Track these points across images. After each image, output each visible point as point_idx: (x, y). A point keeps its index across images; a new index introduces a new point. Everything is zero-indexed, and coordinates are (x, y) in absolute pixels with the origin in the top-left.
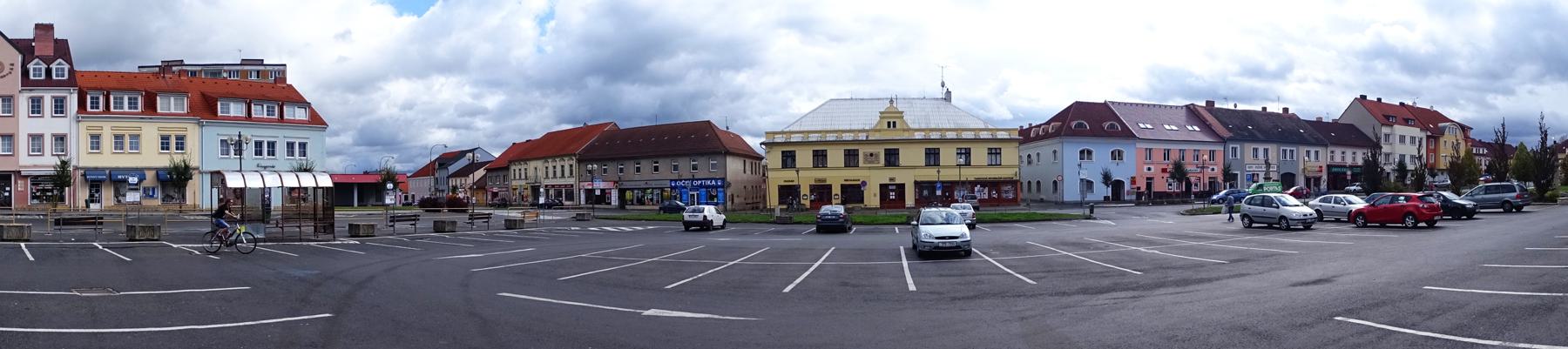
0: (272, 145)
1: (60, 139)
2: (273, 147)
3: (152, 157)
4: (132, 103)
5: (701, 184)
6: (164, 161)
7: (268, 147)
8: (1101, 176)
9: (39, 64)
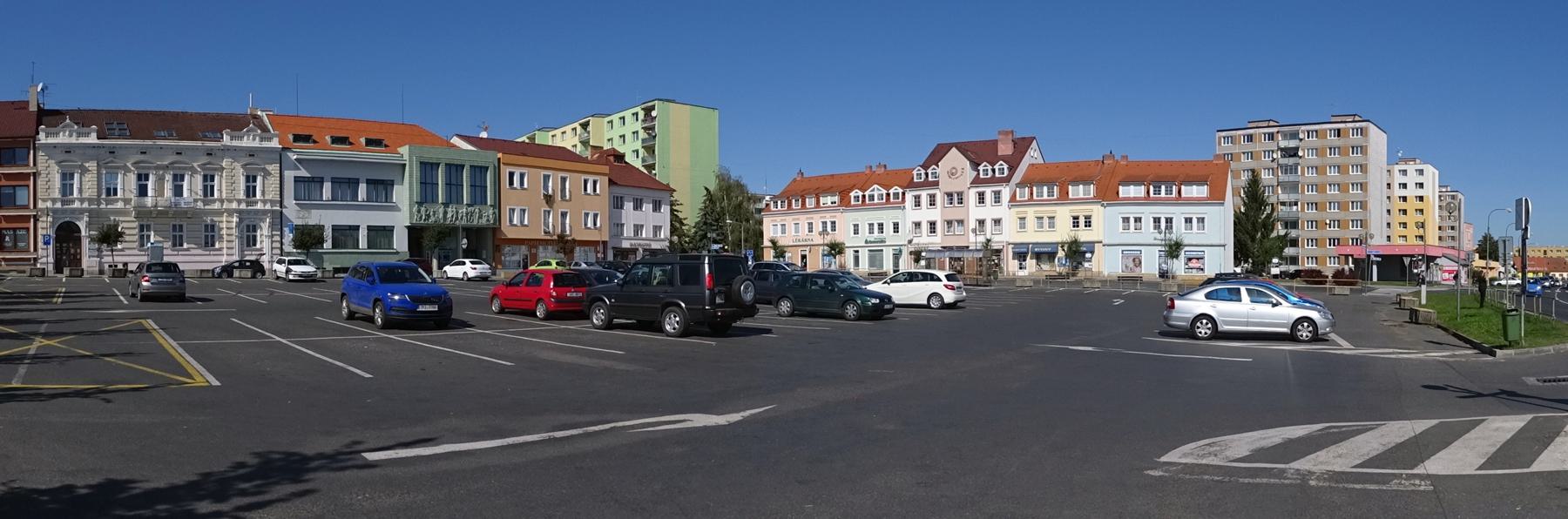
2: (1171, 222)
3: (1062, 233)
4: (1050, 193)
7: (1167, 222)
8: (841, 241)
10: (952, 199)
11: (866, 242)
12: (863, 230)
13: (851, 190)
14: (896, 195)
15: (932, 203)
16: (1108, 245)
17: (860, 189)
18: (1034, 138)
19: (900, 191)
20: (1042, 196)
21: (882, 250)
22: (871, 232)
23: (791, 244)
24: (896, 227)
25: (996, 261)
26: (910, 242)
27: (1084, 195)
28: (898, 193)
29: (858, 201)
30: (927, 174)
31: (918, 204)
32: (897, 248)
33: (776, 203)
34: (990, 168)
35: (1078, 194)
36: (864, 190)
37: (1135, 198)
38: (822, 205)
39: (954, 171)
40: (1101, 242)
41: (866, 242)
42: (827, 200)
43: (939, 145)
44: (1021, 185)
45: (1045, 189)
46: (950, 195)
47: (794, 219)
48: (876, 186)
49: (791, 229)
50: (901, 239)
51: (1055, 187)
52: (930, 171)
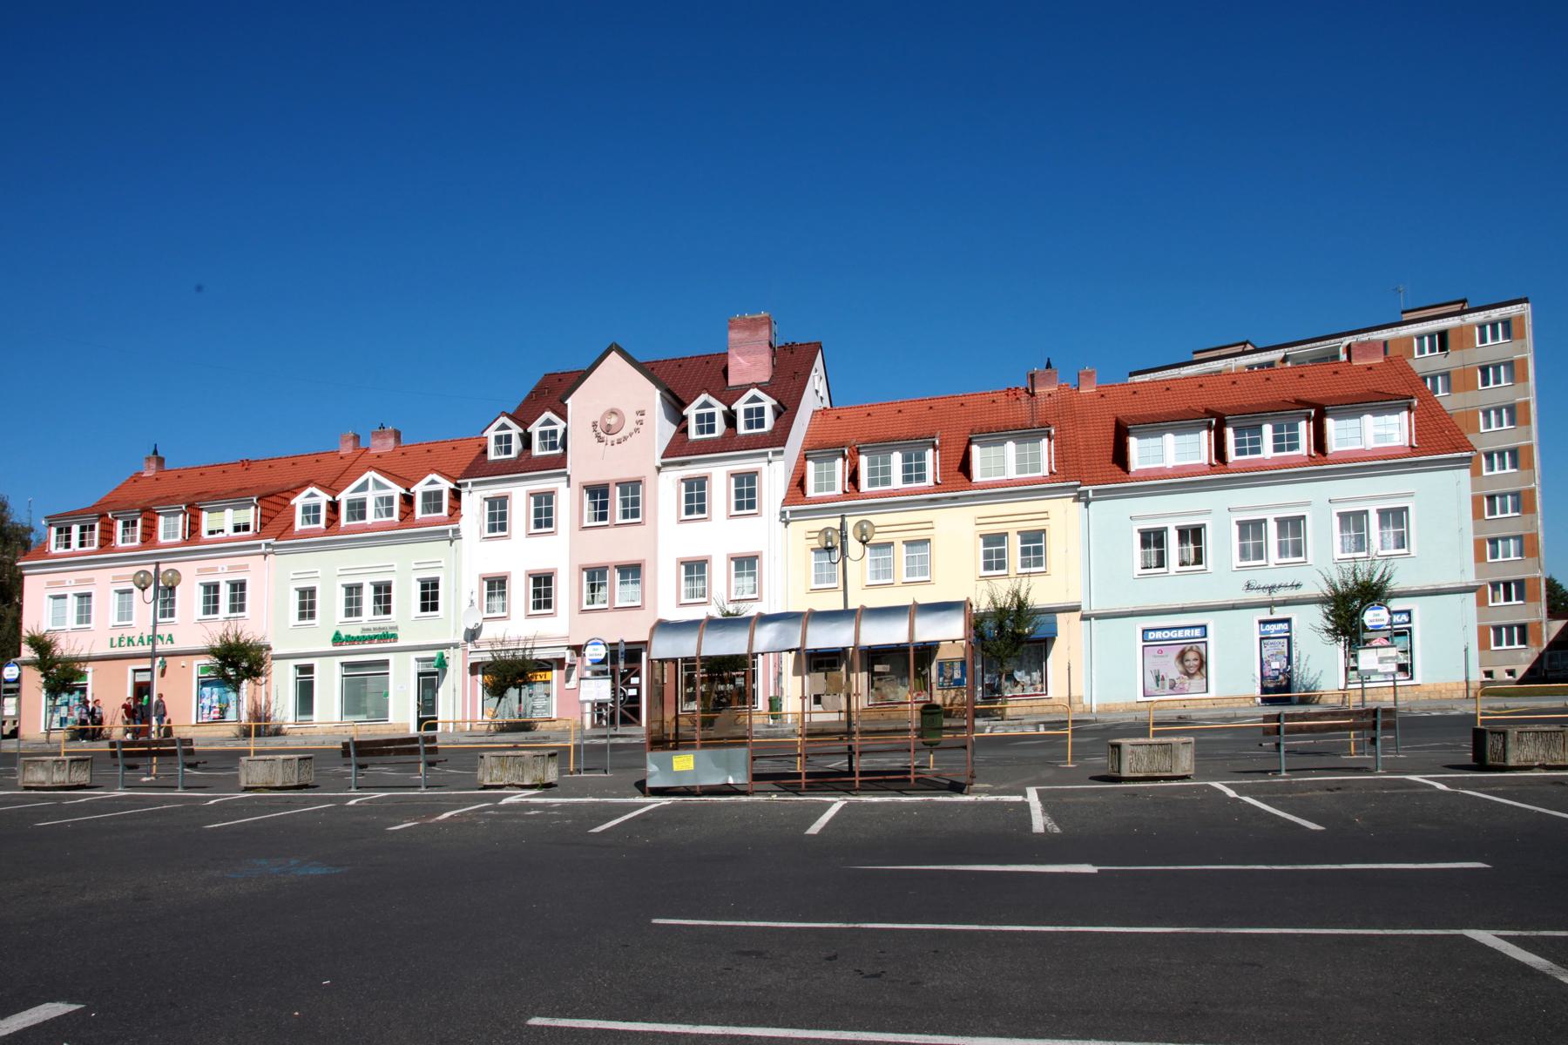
0: (1192, 535)
1: (746, 563)
4: (913, 471)
5: (1192, 648)
6: (986, 594)
9: (759, 400)
10: (604, 505)
11: (337, 639)
12: (331, 604)
13: (295, 491)
14: (433, 500)
15: (544, 516)
16: (1099, 617)
17: (322, 487)
18: (818, 346)
19: (445, 486)
20: (887, 481)
21: (385, 663)
22: (353, 607)
23: (107, 650)
24: (430, 597)
25: (739, 682)
26: (472, 635)
27: (1020, 470)
28: (439, 494)
29: (317, 520)
30: (527, 440)
31: (498, 518)
32: (433, 654)
33: (65, 532)
34: (719, 409)
35: (1003, 471)
36: (332, 488)
37: (1180, 471)
38: (204, 534)
39: (613, 420)
40: (1076, 609)
41: (337, 639)
42: (221, 521)
43: (548, 376)
44: (818, 449)
45: (897, 459)
46: (598, 493)
47: (51, 584)
48: (371, 475)
49: (106, 606)
50: (446, 626)
51: (929, 453)
52: (535, 429)
